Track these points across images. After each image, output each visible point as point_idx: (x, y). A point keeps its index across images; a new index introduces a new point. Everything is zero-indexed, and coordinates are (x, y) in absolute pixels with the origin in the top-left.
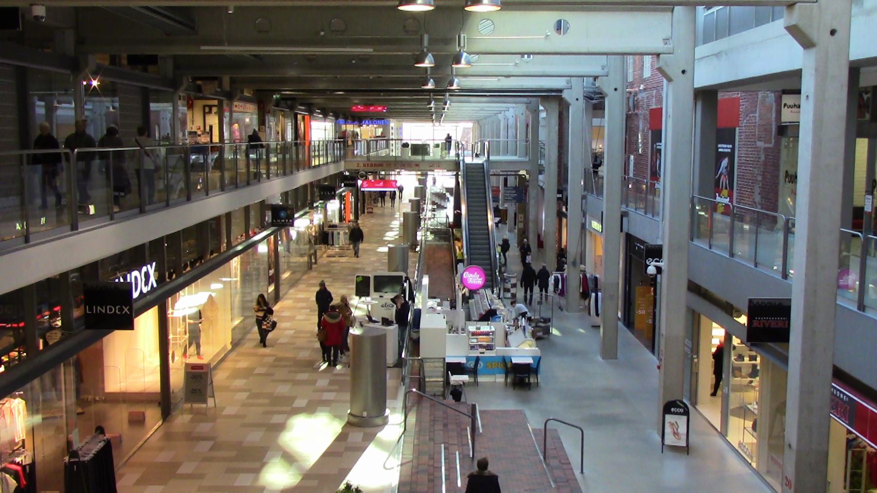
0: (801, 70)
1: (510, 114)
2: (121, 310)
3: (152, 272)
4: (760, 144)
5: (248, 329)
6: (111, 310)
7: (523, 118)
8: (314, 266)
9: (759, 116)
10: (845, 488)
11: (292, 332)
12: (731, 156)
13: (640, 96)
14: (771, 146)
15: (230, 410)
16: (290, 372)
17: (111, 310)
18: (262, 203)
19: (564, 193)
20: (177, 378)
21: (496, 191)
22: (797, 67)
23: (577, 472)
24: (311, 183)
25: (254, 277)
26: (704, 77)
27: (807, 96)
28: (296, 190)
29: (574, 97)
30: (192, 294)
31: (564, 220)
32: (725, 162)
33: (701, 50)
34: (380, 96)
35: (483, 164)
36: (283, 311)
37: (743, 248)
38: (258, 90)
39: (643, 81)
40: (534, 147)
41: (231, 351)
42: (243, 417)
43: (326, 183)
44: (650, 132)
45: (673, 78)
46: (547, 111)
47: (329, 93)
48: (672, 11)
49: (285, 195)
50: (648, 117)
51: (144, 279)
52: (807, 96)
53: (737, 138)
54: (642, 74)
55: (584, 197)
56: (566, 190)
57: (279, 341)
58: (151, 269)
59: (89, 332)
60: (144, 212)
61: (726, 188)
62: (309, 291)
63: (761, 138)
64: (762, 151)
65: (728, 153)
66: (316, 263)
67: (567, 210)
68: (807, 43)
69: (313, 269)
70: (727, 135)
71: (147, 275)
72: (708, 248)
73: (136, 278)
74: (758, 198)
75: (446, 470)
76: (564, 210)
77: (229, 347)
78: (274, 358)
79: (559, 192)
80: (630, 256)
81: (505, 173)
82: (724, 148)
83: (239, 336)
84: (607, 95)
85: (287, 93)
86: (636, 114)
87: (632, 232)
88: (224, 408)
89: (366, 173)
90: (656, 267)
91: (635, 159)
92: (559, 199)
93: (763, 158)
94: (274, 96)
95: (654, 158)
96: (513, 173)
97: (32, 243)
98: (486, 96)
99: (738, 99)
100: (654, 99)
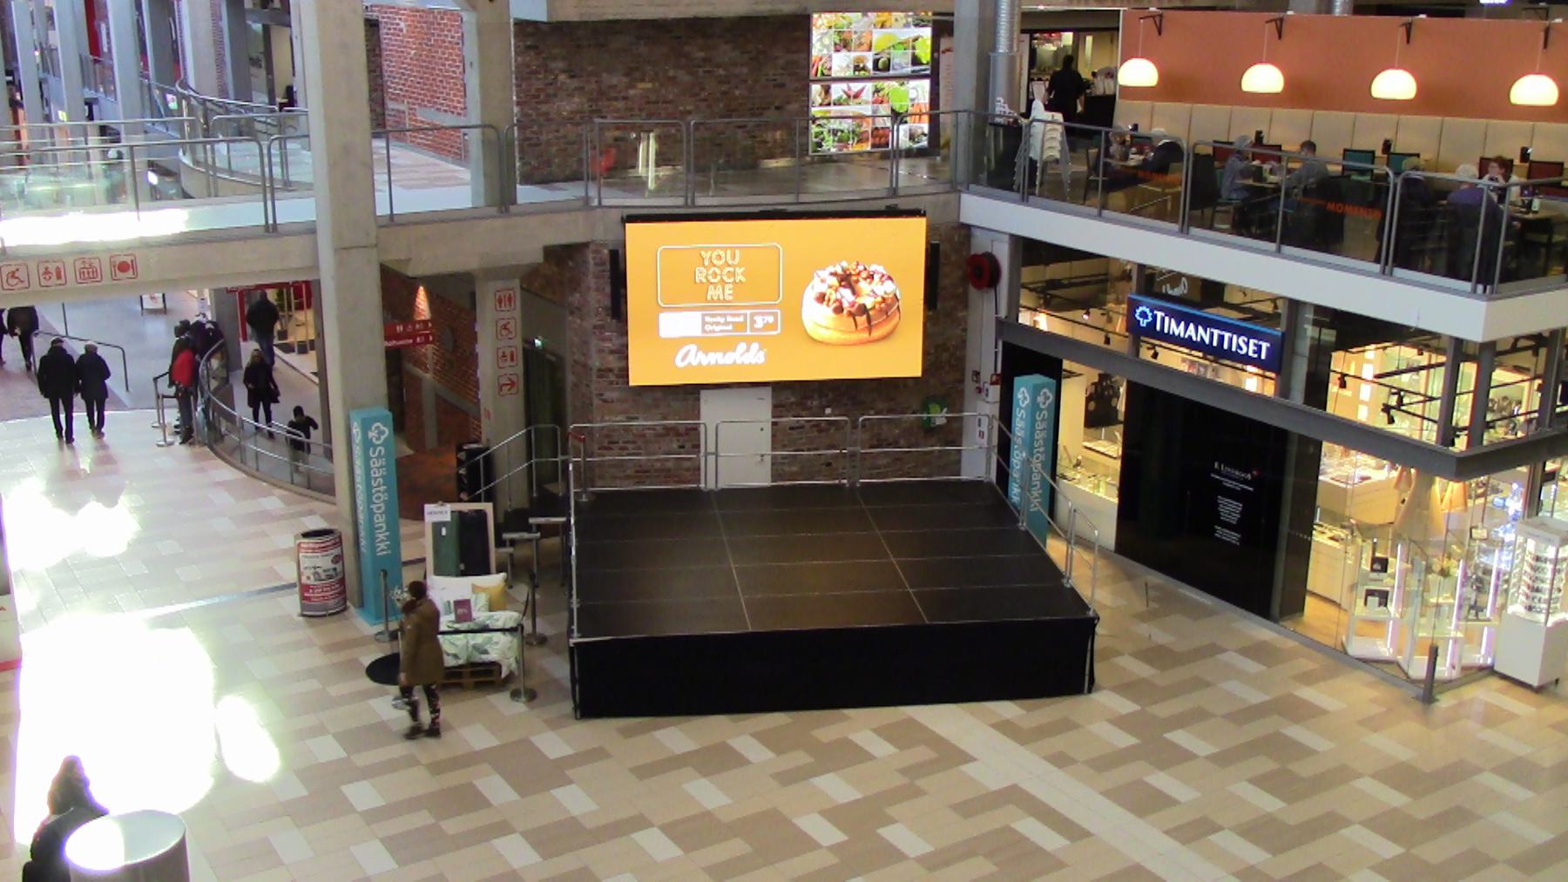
19: (16, 74)
30: (952, 23)
31: (21, 112)
56: (17, 69)
67: (22, 98)
76: (18, 98)
79: (9, 73)
92: (9, 83)
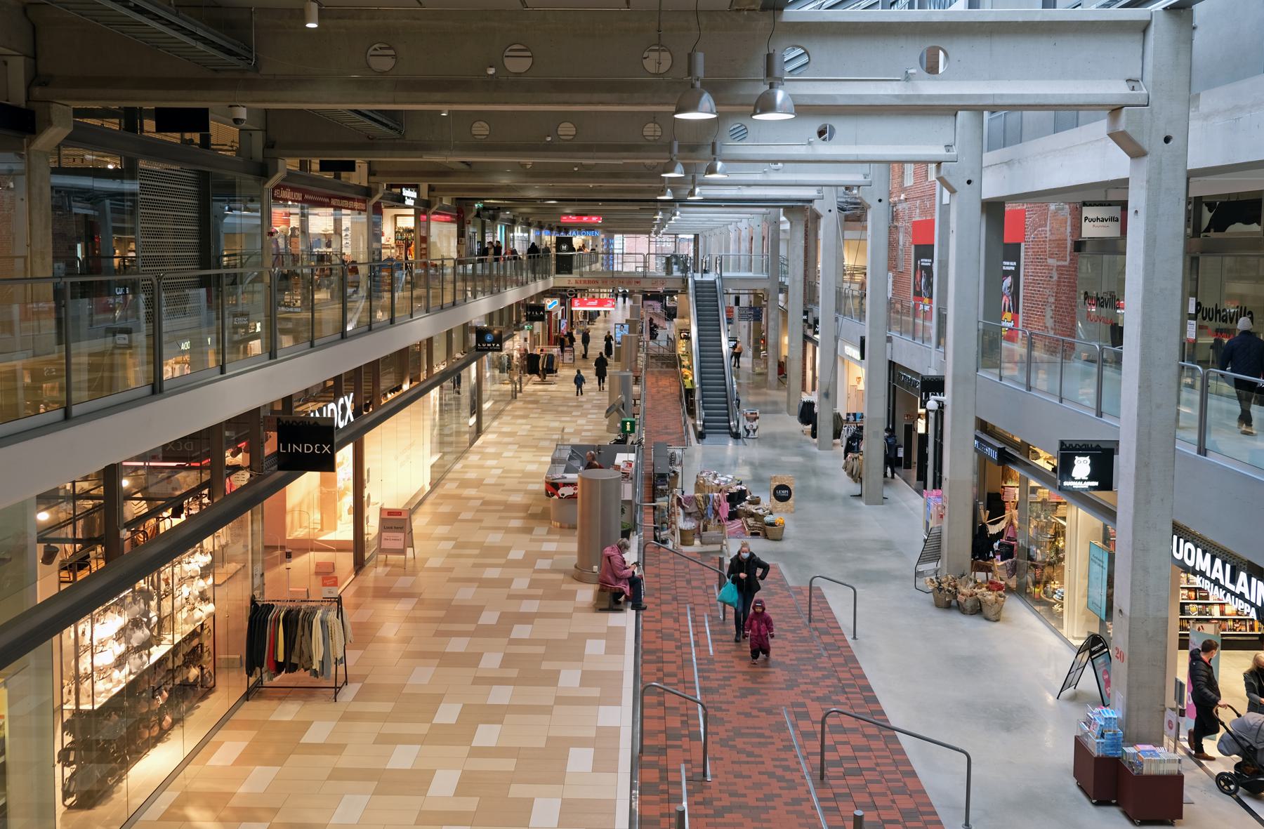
0: (1127, 180)
1: (743, 225)
2: (321, 449)
3: (349, 405)
4: (1051, 261)
5: (448, 467)
6: (307, 448)
7: (759, 230)
8: (519, 395)
9: (1050, 230)
10: (369, 497)
11: (499, 471)
12: (1015, 274)
13: (900, 207)
14: (1066, 263)
15: (434, 562)
16: (500, 518)
17: (308, 448)
18: (465, 325)
20: (372, 526)
21: (729, 311)
22: (1122, 176)
23: (849, 638)
24: (518, 304)
25: (454, 407)
26: (992, 188)
27: (1136, 212)
28: (501, 311)
29: (827, 206)
32: (1008, 281)
33: (988, 157)
34: (598, 205)
35: (715, 282)
36: (486, 447)
37: (1042, 380)
38: (457, 199)
39: (904, 190)
40: (775, 263)
41: (430, 492)
42: (450, 570)
43: (533, 302)
44: (913, 247)
45: (957, 189)
46: (791, 223)
47: (539, 202)
48: (956, 115)
49: (490, 317)
50: (910, 230)
51: (340, 413)
52: (1136, 212)
53: (1022, 254)
54: (902, 182)
55: (837, 319)
57: (485, 482)
58: (348, 401)
59: (280, 474)
60: (346, 338)
61: (1009, 311)
62: (514, 424)
63: (1052, 254)
64: (1054, 270)
65: (1011, 271)
66: (521, 391)
68: (1136, 152)
69: (518, 399)
70: (1012, 252)
71: (344, 408)
72: (998, 380)
73: (332, 410)
74: (1050, 323)
75: (694, 635)
77: (428, 488)
78: (481, 501)
80: (895, 387)
81: (737, 292)
82: (1009, 266)
83: (438, 476)
84: (870, 207)
85: (492, 201)
86: (896, 227)
87: (896, 360)
88: (427, 559)
89: (576, 290)
90: (938, 402)
91: (894, 277)
92: (805, 321)
93: (1055, 277)
94: (476, 205)
95: (918, 276)
96: (747, 292)
97: (228, 374)
98: (720, 206)
99: (1024, 211)
100: (918, 211)
